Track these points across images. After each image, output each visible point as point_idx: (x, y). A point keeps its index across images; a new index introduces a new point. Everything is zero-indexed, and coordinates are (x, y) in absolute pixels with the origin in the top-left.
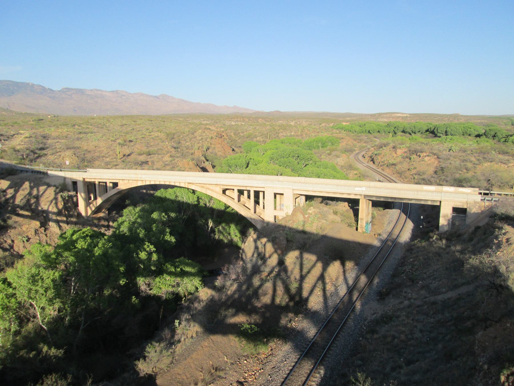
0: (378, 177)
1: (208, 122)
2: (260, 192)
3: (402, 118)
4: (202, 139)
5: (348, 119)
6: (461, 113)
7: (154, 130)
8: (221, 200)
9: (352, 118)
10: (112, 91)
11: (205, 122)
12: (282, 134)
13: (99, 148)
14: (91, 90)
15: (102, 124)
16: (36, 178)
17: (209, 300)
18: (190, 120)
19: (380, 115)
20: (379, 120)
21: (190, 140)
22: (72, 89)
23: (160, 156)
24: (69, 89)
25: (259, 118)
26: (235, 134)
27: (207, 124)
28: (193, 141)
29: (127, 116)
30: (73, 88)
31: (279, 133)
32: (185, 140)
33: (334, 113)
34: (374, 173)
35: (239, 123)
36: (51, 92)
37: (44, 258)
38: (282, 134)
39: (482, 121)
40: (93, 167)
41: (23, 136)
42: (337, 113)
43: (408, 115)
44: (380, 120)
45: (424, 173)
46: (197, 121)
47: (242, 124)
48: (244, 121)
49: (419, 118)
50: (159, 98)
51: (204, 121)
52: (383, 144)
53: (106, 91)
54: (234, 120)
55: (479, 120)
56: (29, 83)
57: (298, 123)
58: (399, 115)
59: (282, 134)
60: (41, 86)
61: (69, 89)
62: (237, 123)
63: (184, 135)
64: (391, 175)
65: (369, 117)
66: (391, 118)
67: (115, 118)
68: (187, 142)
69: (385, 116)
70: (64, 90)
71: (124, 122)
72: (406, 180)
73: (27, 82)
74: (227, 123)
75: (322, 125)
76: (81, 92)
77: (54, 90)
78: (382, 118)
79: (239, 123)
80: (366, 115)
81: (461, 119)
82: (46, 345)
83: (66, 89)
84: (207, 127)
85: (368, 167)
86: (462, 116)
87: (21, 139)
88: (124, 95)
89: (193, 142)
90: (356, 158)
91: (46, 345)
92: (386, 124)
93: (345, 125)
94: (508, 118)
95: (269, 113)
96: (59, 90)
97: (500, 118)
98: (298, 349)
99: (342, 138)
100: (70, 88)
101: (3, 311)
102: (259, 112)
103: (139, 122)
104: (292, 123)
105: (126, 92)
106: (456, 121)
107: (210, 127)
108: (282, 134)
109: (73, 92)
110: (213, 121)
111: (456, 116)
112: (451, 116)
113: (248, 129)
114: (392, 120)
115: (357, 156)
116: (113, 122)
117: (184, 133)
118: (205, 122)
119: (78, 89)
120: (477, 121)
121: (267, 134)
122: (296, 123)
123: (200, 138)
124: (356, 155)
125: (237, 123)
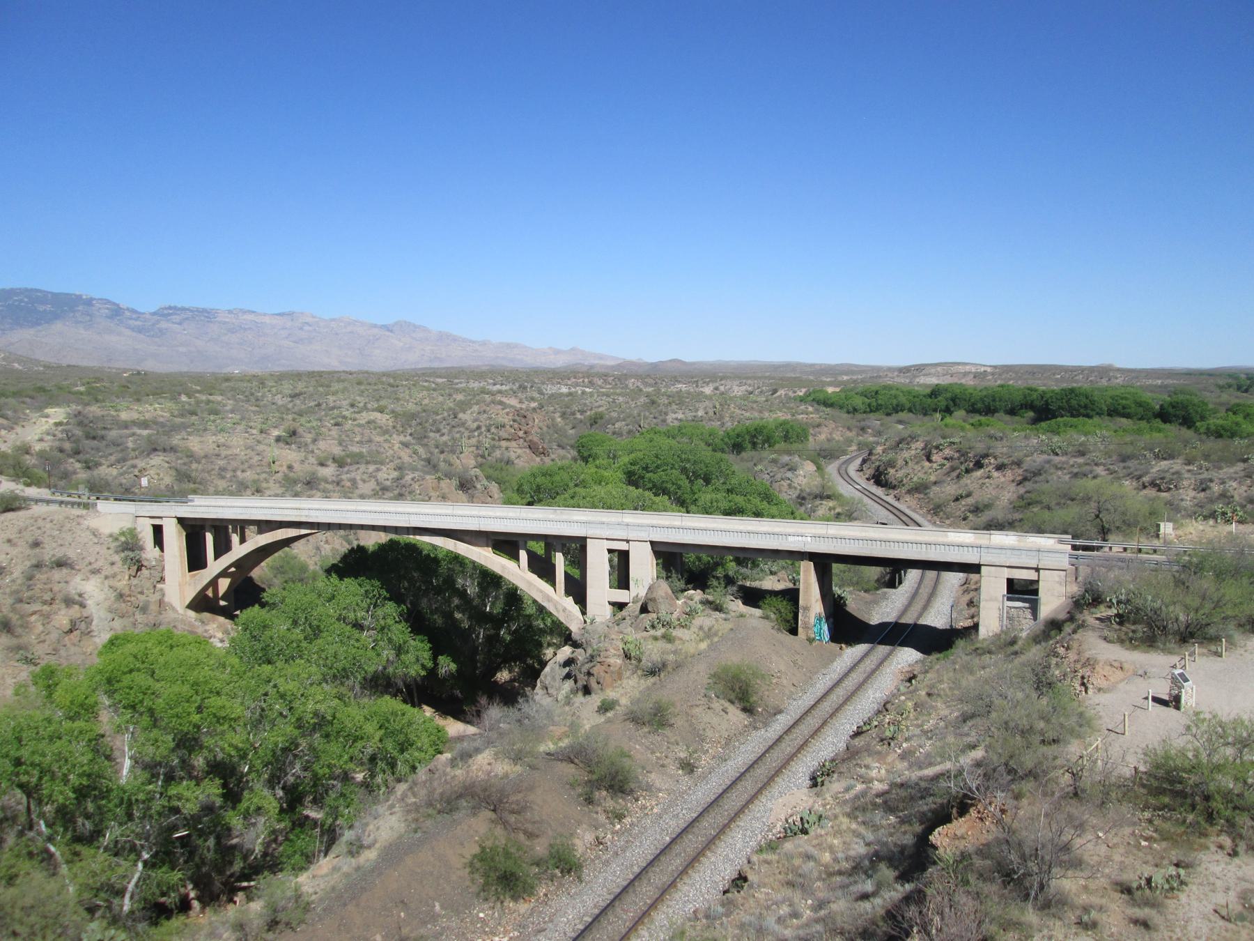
0: (883, 514)
1: (504, 388)
2: (983, 568)
3: (975, 377)
4: (479, 428)
5: (845, 378)
6: (1118, 364)
7: (369, 406)
9: (855, 377)
11: (498, 387)
12: (676, 416)
13: (228, 447)
14: (230, 312)
15: (247, 394)
16: (67, 518)
17: (217, 903)
18: (461, 383)
19: (920, 369)
20: (917, 380)
21: (450, 432)
23: (372, 468)
25: (632, 376)
26: (563, 415)
27: (500, 392)
28: (458, 432)
30: (187, 305)
31: (666, 414)
32: (438, 431)
33: (812, 365)
34: (876, 506)
35: (579, 390)
36: (134, 316)
38: (674, 416)
39: (1166, 382)
40: (204, 492)
41: (51, 421)
42: (821, 365)
43: (989, 370)
44: (922, 382)
45: (988, 506)
46: (475, 385)
47: (584, 392)
48: (591, 384)
49: (1014, 375)
50: (391, 331)
51: (495, 384)
53: (265, 315)
54: (569, 382)
55: (1159, 379)
57: (722, 388)
58: (968, 368)
59: (676, 416)
60: (108, 302)
61: (175, 308)
62: (573, 390)
63: (438, 417)
64: (914, 510)
65: (896, 373)
66: (948, 377)
67: (281, 377)
68: (443, 435)
69: (933, 371)
70: (166, 312)
71: (300, 386)
72: (948, 522)
73: (78, 293)
74: (550, 389)
75: (778, 394)
77: (142, 310)
78: (924, 375)
79: (579, 390)
80: (890, 369)
81: (1117, 378)
82: (483, 701)
83: (170, 308)
84: (499, 398)
85: (864, 491)
86: (1119, 370)
87: (45, 427)
88: (307, 323)
89: (458, 436)
90: (843, 472)
91: (483, 701)
92: (928, 391)
93: (833, 392)
94: (1230, 376)
95: (655, 366)
97: (1211, 374)
99: (819, 426)
100: (179, 306)
102: (632, 363)
103: (336, 386)
104: (708, 390)
106: (1104, 382)
107: (504, 400)
108: (674, 416)
110: (517, 385)
111: (1104, 371)
112: (1092, 370)
113: (597, 404)
114: (944, 381)
115: (844, 466)
116: (272, 387)
117: (438, 414)
118: (498, 387)
120: (1154, 383)
121: (639, 415)
122: (716, 389)
123: (475, 425)
124: (843, 463)
125: (573, 390)
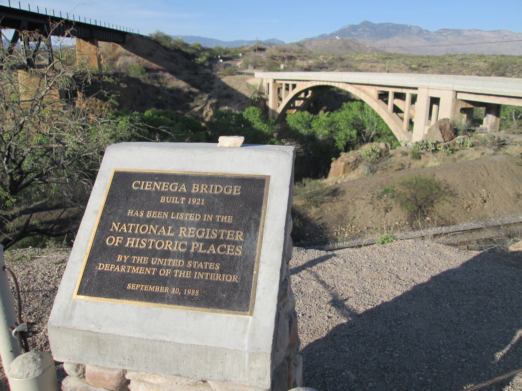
8: (50, 344)
10: (493, 31)
14: (470, 31)
22: (449, 30)
24: (445, 30)
29: (399, 56)
36: (427, 33)
37: (244, 305)
52: (163, 36)
53: (486, 31)
56: (407, 25)
76: (458, 32)
83: (443, 29)
88: (506, 36)
96: (435, 30)
98: (173, 49)
101: (192, 250)
105: (510, 32)
109: (449, 33)
119: (455, 30)
